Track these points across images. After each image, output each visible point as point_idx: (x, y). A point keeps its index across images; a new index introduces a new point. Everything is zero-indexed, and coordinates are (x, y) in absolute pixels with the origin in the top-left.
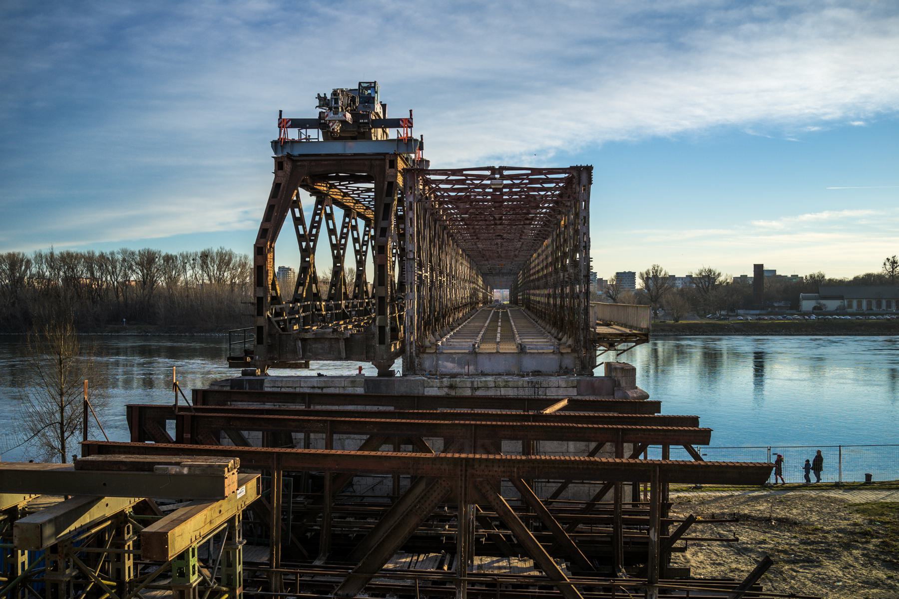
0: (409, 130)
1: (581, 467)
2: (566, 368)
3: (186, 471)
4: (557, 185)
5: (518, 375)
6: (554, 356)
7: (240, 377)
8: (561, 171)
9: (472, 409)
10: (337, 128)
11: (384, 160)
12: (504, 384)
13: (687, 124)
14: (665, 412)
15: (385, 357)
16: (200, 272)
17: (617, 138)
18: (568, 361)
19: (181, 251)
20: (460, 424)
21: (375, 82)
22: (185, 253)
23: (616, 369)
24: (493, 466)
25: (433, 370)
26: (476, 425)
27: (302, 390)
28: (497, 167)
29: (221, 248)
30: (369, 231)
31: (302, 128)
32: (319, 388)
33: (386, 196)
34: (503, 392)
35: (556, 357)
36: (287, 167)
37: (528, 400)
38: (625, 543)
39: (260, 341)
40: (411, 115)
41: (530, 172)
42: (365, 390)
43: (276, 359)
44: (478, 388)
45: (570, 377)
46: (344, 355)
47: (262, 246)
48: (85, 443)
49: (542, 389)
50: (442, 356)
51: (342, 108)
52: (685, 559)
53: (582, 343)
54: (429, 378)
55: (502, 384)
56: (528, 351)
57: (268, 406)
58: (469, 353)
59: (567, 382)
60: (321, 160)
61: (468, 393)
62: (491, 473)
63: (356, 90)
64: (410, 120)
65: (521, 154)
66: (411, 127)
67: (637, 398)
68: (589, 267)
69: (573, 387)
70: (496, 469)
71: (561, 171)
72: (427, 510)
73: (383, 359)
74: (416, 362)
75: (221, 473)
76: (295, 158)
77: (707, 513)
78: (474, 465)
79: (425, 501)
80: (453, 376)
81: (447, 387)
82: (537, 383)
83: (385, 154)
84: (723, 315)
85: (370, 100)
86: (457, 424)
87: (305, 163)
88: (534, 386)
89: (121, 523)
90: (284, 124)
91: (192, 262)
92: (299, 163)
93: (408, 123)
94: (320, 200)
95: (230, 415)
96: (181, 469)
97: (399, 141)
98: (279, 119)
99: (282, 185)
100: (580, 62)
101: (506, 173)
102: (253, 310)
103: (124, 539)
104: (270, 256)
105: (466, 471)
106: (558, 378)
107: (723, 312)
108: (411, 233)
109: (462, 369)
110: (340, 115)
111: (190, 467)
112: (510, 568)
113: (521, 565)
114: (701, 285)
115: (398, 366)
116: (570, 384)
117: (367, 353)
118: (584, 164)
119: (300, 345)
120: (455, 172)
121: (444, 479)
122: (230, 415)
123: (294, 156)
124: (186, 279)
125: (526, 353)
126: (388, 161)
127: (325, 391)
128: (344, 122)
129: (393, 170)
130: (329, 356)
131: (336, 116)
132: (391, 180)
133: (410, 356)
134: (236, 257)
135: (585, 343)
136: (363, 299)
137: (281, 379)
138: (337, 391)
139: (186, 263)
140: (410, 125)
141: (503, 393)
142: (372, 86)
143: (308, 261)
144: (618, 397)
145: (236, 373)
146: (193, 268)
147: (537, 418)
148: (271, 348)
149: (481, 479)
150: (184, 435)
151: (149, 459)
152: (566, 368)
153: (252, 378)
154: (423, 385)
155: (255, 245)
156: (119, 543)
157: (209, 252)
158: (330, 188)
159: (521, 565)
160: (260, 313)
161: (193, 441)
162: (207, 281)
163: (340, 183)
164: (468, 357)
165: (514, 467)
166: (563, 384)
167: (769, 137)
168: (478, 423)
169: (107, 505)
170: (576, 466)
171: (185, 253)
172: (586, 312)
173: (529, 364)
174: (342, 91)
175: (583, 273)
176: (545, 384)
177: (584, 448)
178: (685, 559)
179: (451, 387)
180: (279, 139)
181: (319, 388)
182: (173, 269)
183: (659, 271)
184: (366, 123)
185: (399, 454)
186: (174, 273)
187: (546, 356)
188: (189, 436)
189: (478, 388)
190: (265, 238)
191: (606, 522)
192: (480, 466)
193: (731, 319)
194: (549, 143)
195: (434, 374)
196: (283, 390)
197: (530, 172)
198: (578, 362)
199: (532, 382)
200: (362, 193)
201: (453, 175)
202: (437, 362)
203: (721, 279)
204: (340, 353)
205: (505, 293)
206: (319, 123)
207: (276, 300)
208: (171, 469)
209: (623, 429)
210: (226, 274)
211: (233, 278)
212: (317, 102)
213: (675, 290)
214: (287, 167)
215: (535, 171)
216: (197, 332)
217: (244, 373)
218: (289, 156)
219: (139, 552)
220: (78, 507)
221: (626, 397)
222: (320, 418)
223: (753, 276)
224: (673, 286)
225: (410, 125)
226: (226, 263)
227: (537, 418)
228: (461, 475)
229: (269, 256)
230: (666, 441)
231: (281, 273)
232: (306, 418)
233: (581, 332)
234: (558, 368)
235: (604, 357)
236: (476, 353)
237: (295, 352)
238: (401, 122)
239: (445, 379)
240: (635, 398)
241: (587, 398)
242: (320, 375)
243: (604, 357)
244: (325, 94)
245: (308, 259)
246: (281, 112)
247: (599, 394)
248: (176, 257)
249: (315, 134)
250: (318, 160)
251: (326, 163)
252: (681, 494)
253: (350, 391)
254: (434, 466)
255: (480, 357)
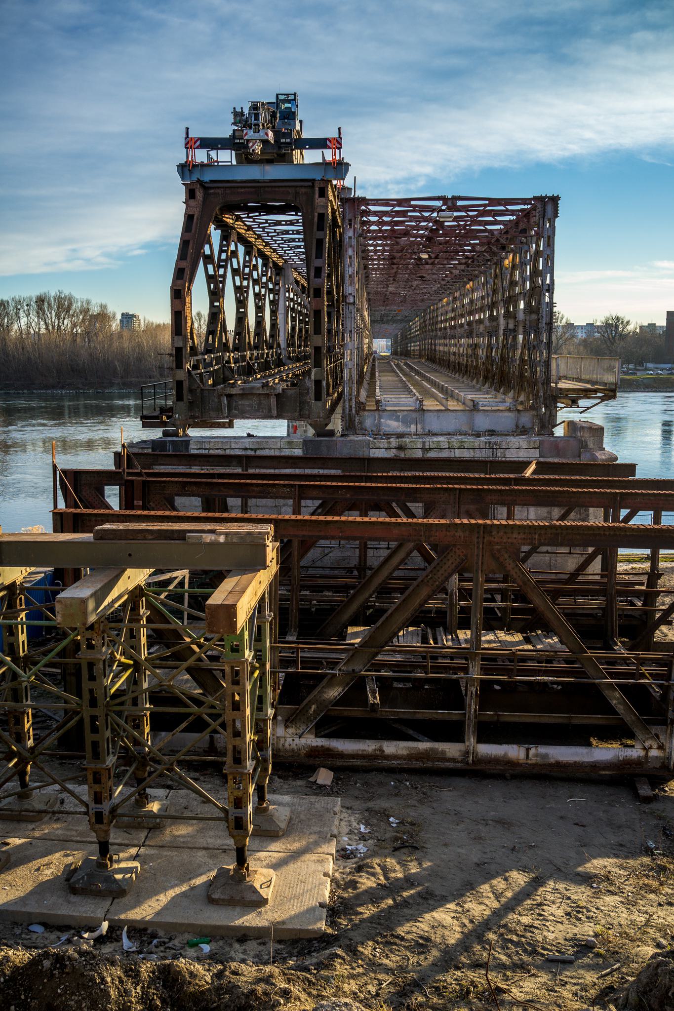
0: (338, 151)
1: (608, 533)
2: (523, 427)
3: (222, 539)
4: (380, 218)
5: (473, 435)
6: (510, 414)
7: (161, 438)
8: (520, 201)
9: (423, 472)
10: (258, 148)
11: (313, 187)
12: (459, 444)
13: (575, 149)
14: (639, 475)
15: (322, 415)
16: (36, 320)
17: (497, 164)
18: (526, 419)
19: (13, 296)
20: (442, 489)
21: (295, 94)
22: (17, 298)
23: (583, 428)
24: (512, 533)
25: (374, 429)
26: (460, 489)
27: (232, 452)
28: (450, 197)
29: (59, 291)
30: (267, 272)
31: (213, 149)
32: (252, 449)
33: (318, 230)
34: (458, 454)
35: (511, 415)
36: (199, 194)
37: (491, 462)
38: (620, 616)
39: (180, 397)
40: (340, 133)
41: (487, 202)
42: (303, 451)
43: (197, 417)
44: (430, 449)
45: (530, 437)
46: (275, 412)
47: (180, 288)
48: (55, 511)
49: (502, 450)
50: (386, 413)
51: (263, 125)
52: (662, 633)
53: (542, 399)
54: (375, 438)
55: (456, 445)
56: (481, 408)
57: (195, 469)
58: (416, 411)
59: (529, 442)
60: (238, 187)
61: (419, 454)
62: (510, 540)
63: (274, 103)
64: (339, 140)
65: (387, 183)
66: (340, 148)
67: (606, 460)
68: (551, 314)
69: (535, 448)
70: (515, 535)
71: (520, 201)
72: (440, 580)
73: (319, 417)
74: (357, 421)
75: (261, 541)
76: (207, 185)
77: (670, 585)
78: (491, 532)
79: (438, 571)
80: (400, 436)
81: (395, 448)
82: (495, 443)
83: (313, 181)
84: (631, 369)
85: (290, 115)
86: (439, 489)
87: (219, 191)
88: (492, 446)
89: (136, 597)
90: (190, 144)
91: (26, 308)
92: (212, 191)
93: (337, 143)
94: (225, 234)
95: (185, 480)
96: (217, 537)
97: (325, 164)
98: (186, 138)
99: (195, 217)
100: (449, 75)
101: (459, 203)
102: (168, 361)
103: (139, 615)
104: (188, 299)
105: (484, 538)
106: (517, 438)
107: (631, 366)
108: (350, 273)
109: (406, 427)
110: (262, 133)
111: (227, 534)
112: (500, 642)
113: (509, 638)
114: (606, 335)
115: (336, 424)
116: (532, 445)
117: (301, 410)
118: (550, 194)
119: (226, 402)
120: (401, 202)
121: (459, 547)
122: (185, 480)
123: (205, 183)
124: (20, 329)
125: (479, 410)
126: (317, 189)
127: (259, 453)
128: (265, 142)
129: (323, 199)
130: (258, 414)
131: (257, 134)
132: (321, 212)
133: (349, 414)
134: (77, 302)
135: (545, 399)
136: (263, 350)
137: (208, 440)
138: (272, 453)
139: (19, 309)
140: (338, 146)
141: (457, 455)
142: (292, 98)
143: (217, 306)
144: (585, 459)
145: (156, 434)
146: (27, 316)
147: (518, 481)
148: (191, 405)
149: (499, 547)
150: (135, 502)
151: (176, 526)
152: (523, 427)
153: (174, 438)
154: (369, 446)
155: (172, 288)
156: (136, 618)
157: (46, 296)
158: (237, 220)
159: (509, 638)
160: (179, 365)
161: (144, 508)
162: (43, 331)
163: (248, 214)
164: (414, 415)
165: (535, 533)
166: (525, 445)
167: (669, 164)
168: (463, 486)
169: (129, 578)
170: (602, 533)
171: (17, 298)
172: (547, 364)
173: (482, 422)
174: (263, 104)
175: (545, 320)
176: (503, 445)
177: (546, 515)
178: (662, 633)
179: (400, 448)
180: (186, 162)
181: (252, 449)
182: (5, 317)
183: (559, 319)
184: (288, 143)
185: (365, 519)
186: (6, 321)
187: (501, 414)
188: (140, 503)
189: (430, 449)
190: (182, 279)
191: (593, 593)
192: (498, 532)
193: (639, 373)
194: (417, 169)
195: (378, 434)
196: (212, 452)
197: (487, 202)
198: (536, 420)
199: (490, 443)
200: (270, 226)
201: (399, 206)
202: (379, 420)
203: (630, 328)
204: (270, 410)
205: (381, 343)
206: (232, 143)
207: (194, 350)
208: (206, 538)
209: (621, 494)
210: (66, 322)
211: (74, 325)
212: (231, 118)
213: (576, 341)
214: (199, 194)
215: (493, 201)
216: (36, 389)
217: (165, 434)
218: (200, 183)
219: (477, 617)
220: (110, 581)
221: (595, 458)
222: (286, 482)
223: (665, 324)
224: (573, 336)
225: (338, 146)
226: (66, 309)
227: (518, 481)
228: (478, 543)
229: (187, 299)
230: (612, 504)
231: (125, 320)
232: (271, 482)
233: (541, 387)
234: (514, 427)
235: (565, 414)
236: (423, 410)
237: (219, 409)
238: (328, 143)
239: (392, 440)
240: (603, 460)
241: (550, 460)
242: (249, 435)
243: (565, 414)
244: (242, 108)
245: (216, 304)
246: (187, 129)
247: (564, 456)
248: (8, 302)
249: (226, 157)
250: (234, 187)
251: (243, 190)
252: (635, 565)
253: (287, 452)
254: (448, 533)
255: (427, 415)
